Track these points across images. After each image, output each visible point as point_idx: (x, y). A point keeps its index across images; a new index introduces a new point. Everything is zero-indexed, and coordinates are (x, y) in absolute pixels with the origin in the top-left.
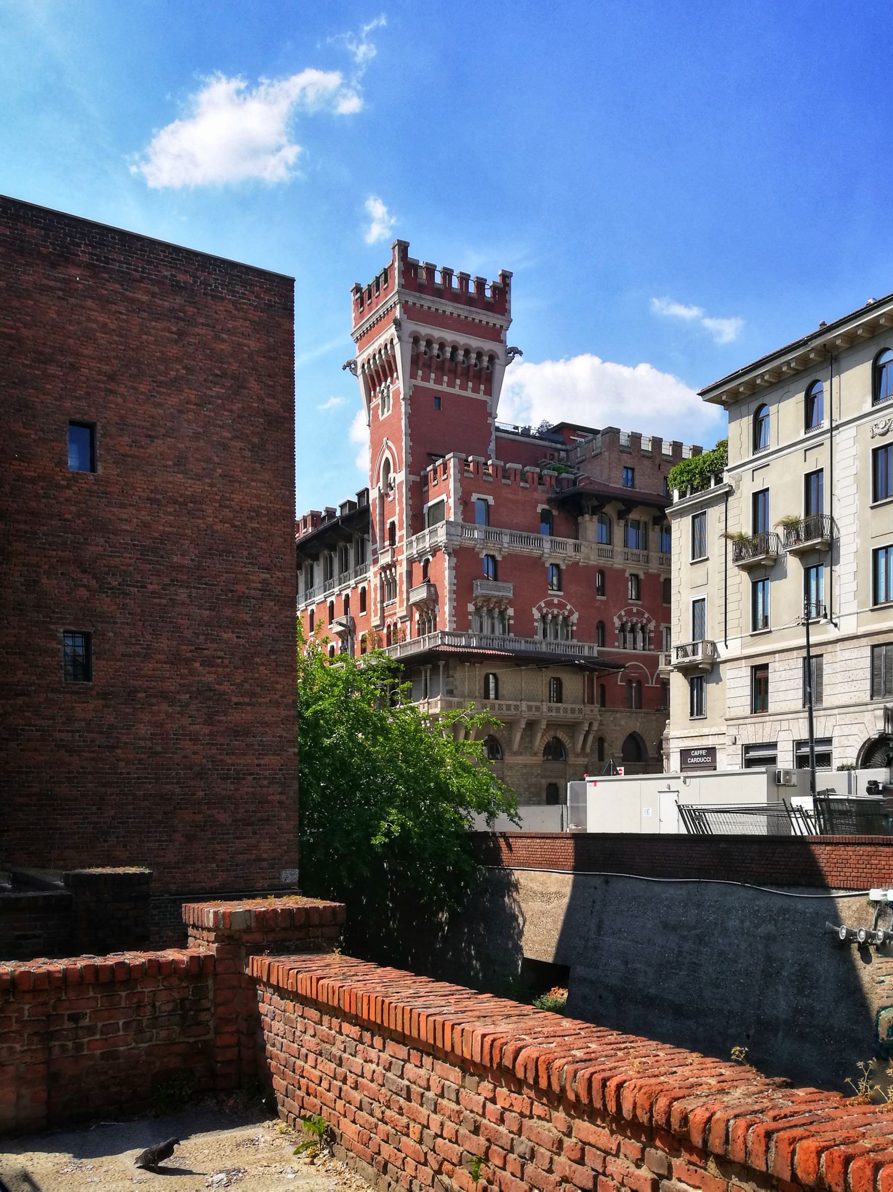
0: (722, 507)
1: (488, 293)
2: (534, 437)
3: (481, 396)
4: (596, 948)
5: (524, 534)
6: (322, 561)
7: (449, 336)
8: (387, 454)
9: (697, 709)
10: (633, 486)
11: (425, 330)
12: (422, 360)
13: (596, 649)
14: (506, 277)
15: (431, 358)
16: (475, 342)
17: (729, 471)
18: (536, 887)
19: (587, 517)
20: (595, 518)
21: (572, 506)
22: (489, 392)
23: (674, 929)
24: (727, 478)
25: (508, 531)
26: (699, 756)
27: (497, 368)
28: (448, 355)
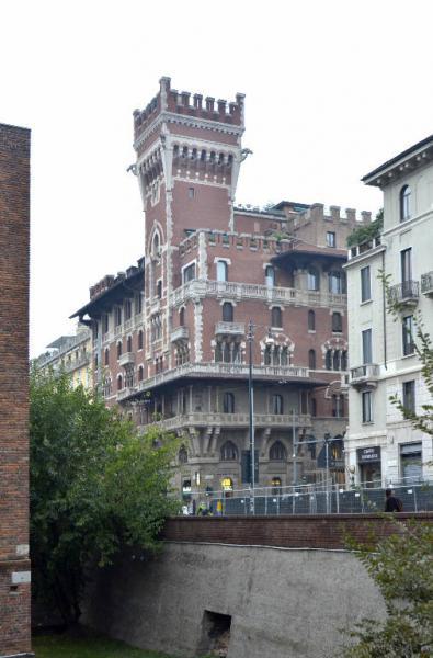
0: (381, 258)
1: (227, 110)
2: (262, 213)
3: (223, 185)
4: (248, 601)
5: (253, 285)
6: (113, 314)
8: (157, 231)
9: (366, 419)
10: (334, 246)
11: (182, 141)
13: (308, 371)
14: (240, 98)
15: (187, 159)
16: (219, 147)
17: (385, 235)
18: (214, 557)
19: (300, 271)
21: (289, 265)
22: (229, 182)
23: (295, 586)
24: (383, 241)
25: (241, 284)
26: (370, 454)
27: (235, 164)
28: (199, 157)
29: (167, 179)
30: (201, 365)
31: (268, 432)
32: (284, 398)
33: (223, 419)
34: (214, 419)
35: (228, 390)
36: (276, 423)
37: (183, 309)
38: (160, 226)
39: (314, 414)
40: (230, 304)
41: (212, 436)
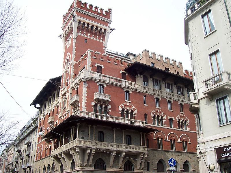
7: (91, 22)
11: (83, 19)
12: (82, 27)
14: (109, 9)
20: (142, 76)
22: (104, 40)
29: (74, 34)
30: (83, 112)
31: (123, 154)
32: (132, 136)
33: (97, 145)
34: (92, 144)
35: (101, 128)
36: (118, 149)
37: (77, 88)
38: (70, 55)
39: (148, 147)
40: (101, 67)
41: (90, 154)
